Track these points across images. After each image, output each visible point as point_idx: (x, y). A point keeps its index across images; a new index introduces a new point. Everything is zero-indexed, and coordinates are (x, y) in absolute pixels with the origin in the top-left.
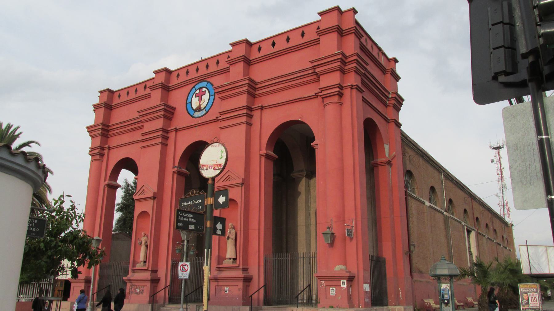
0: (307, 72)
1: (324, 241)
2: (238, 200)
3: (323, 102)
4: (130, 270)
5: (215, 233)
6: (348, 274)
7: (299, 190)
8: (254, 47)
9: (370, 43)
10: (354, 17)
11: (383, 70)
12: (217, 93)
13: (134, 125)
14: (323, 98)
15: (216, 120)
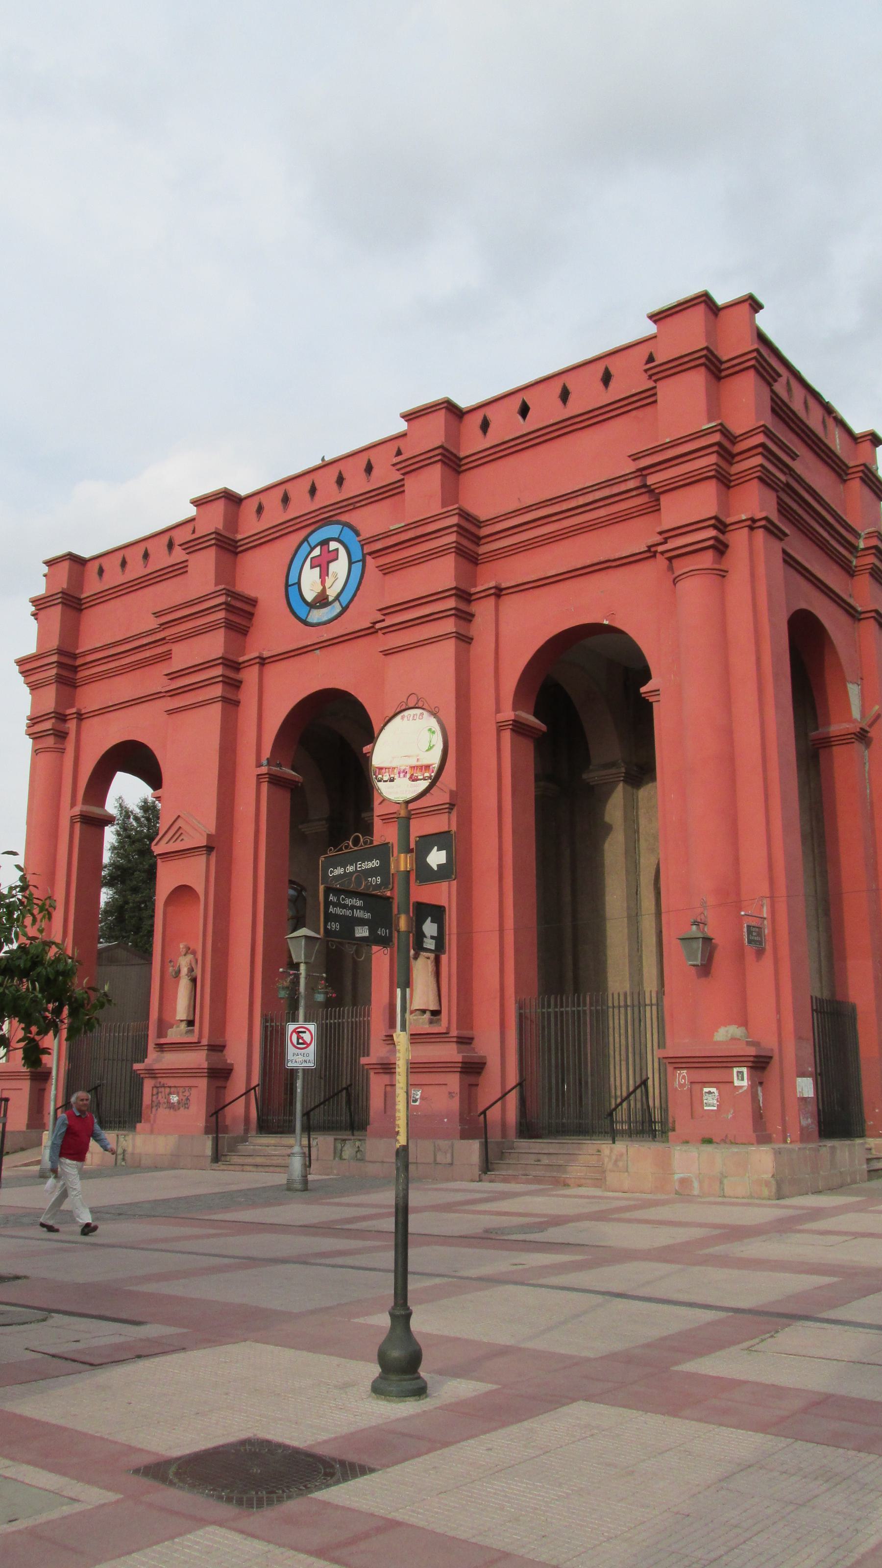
0: (623, 487)
1: (681, 961)
3: (671, 569)
5: (419, 947)
6: (752, 1051)
7: (607, 819)
8: (468, 419)
9: (799, 393)
10: (753, 319)
11: (839, 469)
12: (370, 554)
13: (146, 651)
14: (670, 559)
15: (371, 631)
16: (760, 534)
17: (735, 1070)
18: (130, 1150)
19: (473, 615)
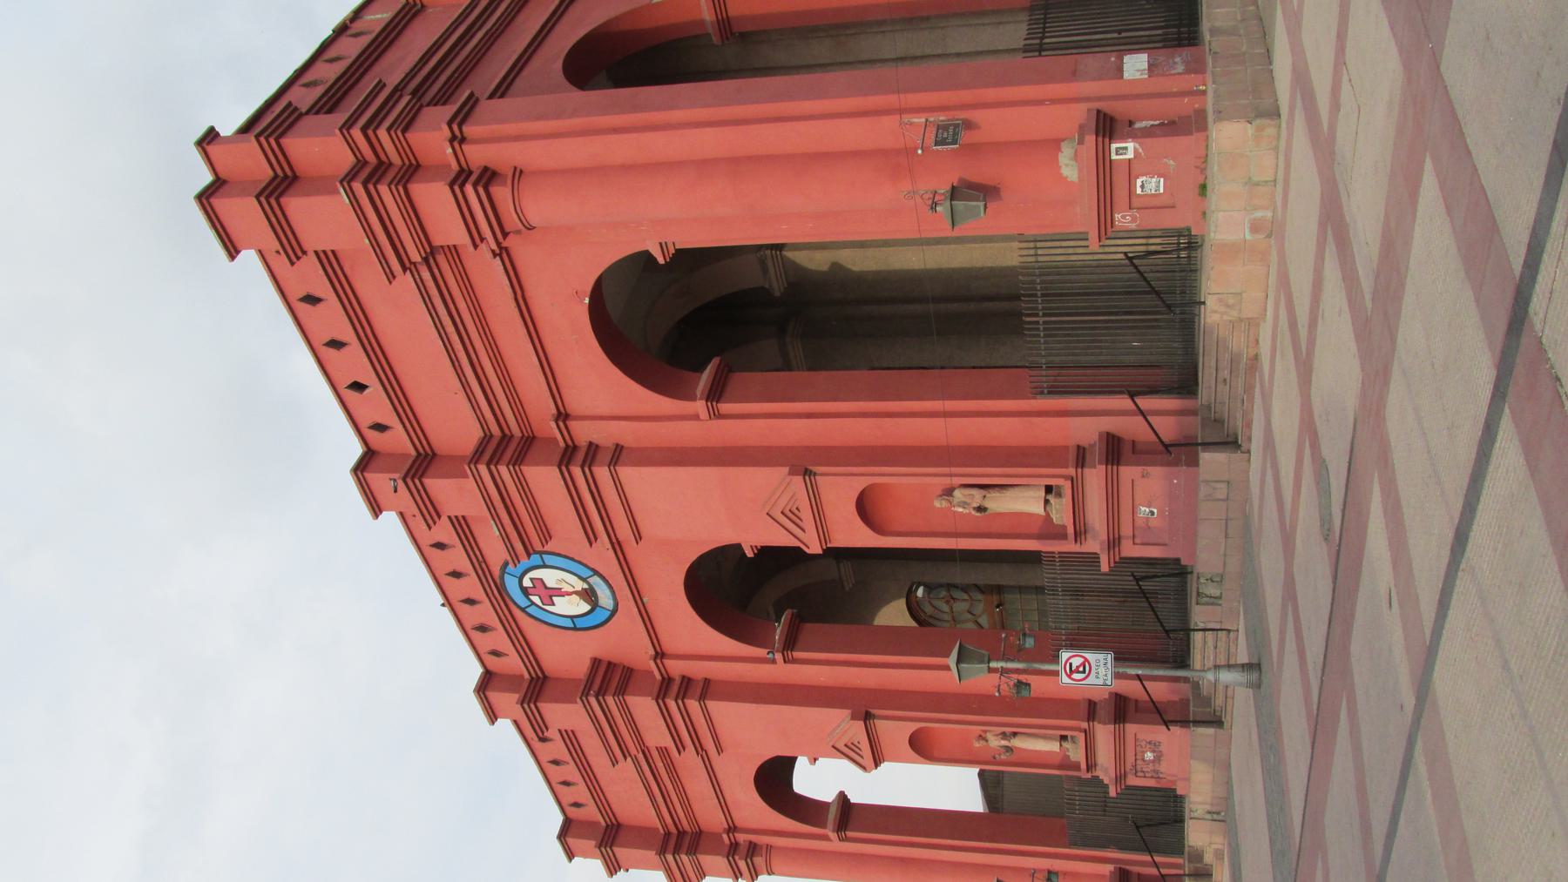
1: (978, 217)
2: (860, 484)
3: (518, 232)
4: (1076, 548)
6: (1090, 139)
7: (825, 268)
10: (228, 140)
13: (659, 771)
16: (468, 130)
17: (1114, 157)
18: (1208, 808)
19: (591, 444)
